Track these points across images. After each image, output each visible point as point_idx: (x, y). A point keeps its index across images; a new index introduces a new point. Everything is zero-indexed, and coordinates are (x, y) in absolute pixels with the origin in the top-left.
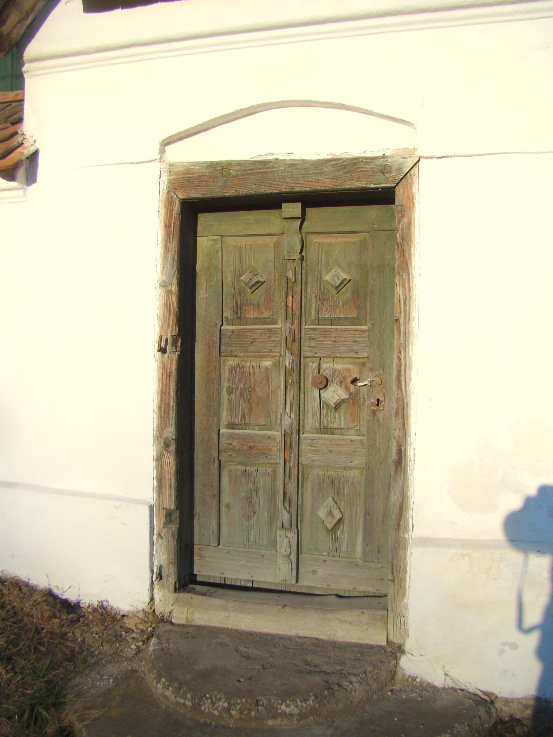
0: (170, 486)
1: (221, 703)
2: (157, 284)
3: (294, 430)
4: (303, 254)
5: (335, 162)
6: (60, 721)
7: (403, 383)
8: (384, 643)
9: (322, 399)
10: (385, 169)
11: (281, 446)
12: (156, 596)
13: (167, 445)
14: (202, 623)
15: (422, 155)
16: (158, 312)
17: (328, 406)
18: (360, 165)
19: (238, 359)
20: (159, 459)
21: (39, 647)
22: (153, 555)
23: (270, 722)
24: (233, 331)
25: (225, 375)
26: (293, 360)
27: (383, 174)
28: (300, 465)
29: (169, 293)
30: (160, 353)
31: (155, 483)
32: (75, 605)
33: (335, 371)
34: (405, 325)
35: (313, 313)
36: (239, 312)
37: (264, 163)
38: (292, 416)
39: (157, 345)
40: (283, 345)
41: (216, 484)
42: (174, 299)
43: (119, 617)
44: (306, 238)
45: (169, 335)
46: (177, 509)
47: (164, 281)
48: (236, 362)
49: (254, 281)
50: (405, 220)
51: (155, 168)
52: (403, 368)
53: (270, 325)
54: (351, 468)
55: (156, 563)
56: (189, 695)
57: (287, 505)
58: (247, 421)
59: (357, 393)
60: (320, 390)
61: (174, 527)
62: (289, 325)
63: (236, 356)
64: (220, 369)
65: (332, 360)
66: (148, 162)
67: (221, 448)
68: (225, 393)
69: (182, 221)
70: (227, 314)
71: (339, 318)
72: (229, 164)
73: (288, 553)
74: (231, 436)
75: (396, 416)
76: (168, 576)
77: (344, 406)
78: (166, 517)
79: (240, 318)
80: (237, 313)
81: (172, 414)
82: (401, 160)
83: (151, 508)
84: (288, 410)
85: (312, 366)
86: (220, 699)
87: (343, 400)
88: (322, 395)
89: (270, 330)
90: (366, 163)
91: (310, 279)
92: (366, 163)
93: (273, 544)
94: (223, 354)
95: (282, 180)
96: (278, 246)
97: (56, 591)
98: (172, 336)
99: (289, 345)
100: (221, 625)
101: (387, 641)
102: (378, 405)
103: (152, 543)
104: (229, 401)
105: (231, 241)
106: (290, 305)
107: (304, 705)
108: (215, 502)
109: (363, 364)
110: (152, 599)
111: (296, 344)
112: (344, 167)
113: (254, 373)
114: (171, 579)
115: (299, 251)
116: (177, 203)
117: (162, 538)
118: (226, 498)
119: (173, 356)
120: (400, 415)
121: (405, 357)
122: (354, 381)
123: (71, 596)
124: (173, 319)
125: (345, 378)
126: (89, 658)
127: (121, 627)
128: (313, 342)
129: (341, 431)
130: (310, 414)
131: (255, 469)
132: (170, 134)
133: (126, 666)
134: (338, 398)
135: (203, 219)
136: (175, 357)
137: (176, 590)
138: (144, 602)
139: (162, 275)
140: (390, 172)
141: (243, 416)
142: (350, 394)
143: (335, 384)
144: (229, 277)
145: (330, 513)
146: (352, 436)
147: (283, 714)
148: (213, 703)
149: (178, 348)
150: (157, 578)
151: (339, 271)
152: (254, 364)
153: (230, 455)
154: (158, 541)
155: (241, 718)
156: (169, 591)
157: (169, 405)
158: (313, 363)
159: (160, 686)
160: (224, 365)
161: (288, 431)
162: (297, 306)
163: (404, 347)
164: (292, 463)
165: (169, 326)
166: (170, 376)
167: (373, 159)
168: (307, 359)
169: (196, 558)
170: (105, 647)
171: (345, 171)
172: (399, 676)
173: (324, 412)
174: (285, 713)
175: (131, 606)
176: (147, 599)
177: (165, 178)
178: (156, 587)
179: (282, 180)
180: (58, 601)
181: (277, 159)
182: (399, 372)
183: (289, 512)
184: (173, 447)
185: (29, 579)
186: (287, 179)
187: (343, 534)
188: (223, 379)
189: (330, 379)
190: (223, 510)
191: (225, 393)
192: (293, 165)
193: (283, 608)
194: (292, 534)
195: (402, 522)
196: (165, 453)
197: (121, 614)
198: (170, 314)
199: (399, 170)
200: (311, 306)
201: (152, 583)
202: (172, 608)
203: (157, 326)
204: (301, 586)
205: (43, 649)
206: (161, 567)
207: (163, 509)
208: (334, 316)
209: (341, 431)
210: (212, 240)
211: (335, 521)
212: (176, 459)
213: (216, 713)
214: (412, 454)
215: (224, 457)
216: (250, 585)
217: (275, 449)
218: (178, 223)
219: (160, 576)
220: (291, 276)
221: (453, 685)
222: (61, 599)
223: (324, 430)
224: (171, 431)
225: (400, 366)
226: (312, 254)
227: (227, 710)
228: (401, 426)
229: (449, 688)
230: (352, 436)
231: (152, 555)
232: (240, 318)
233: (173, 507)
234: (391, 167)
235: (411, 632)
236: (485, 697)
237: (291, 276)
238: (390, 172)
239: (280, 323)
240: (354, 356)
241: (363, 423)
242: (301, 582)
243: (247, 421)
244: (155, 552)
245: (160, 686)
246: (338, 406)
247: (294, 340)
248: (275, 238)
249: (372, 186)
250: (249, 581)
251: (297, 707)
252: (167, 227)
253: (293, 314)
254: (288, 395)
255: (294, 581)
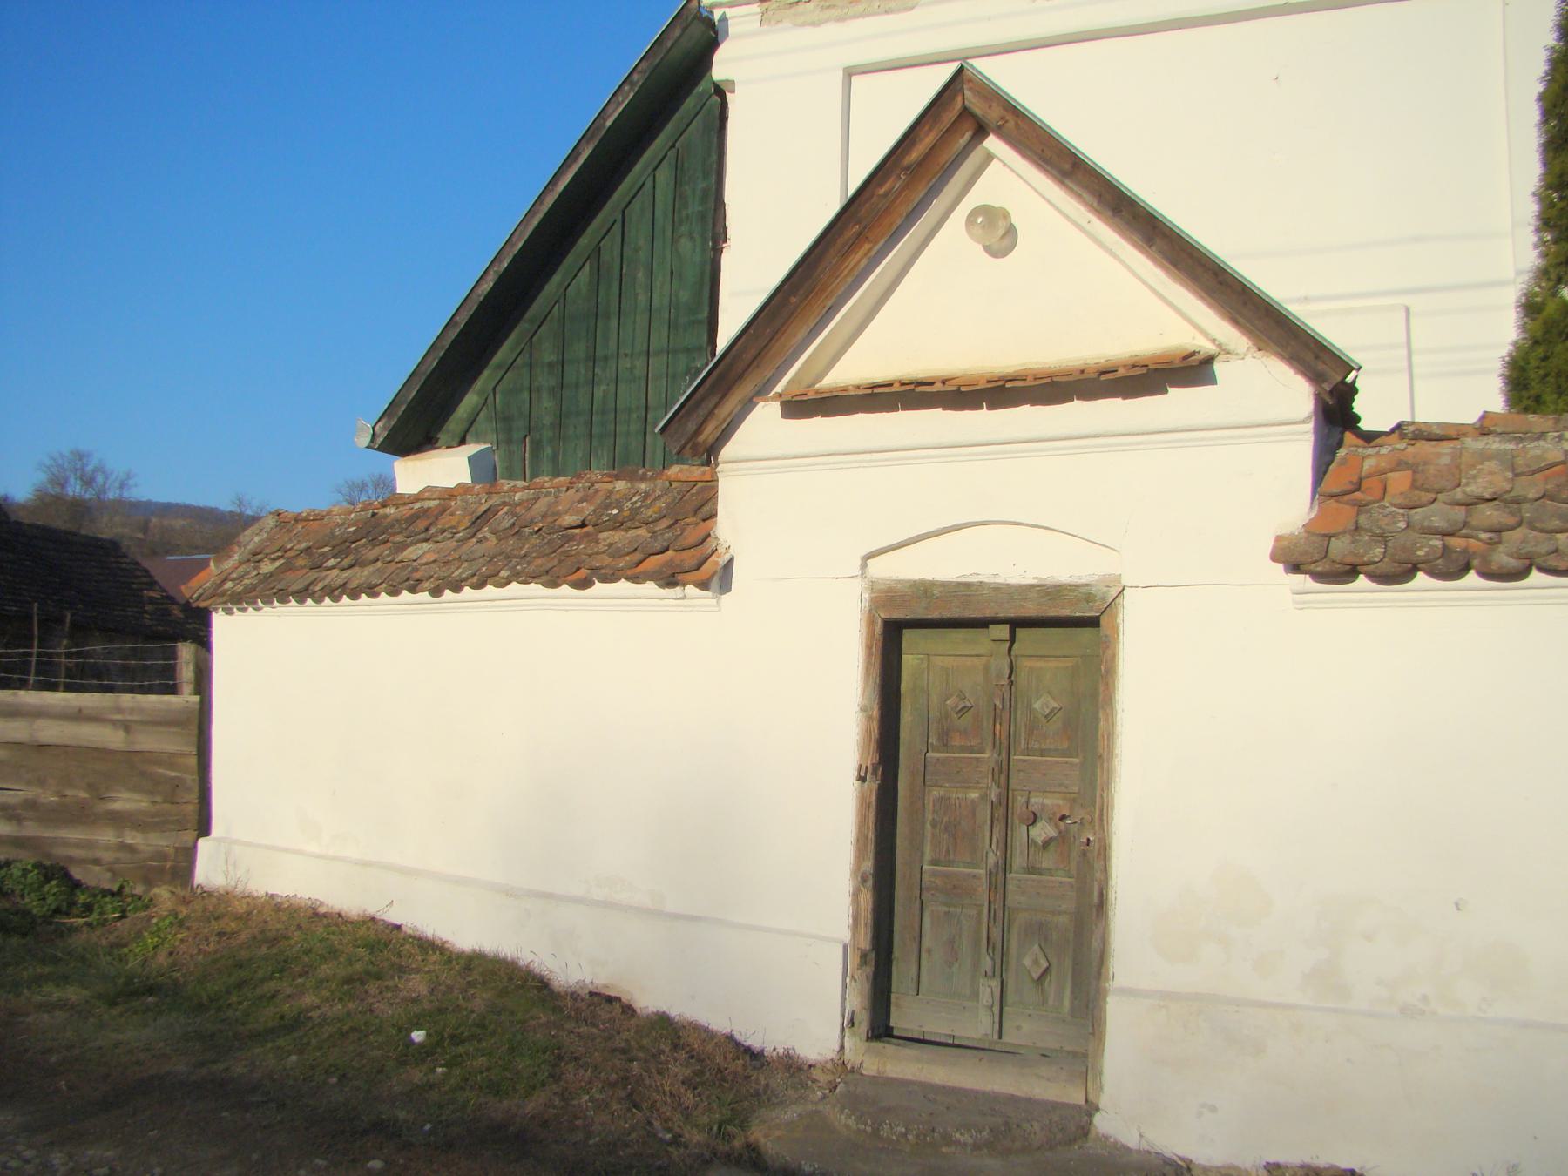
0: (866, 924)
1: (899, 1129)
2: (858, 709)
3: (1000, 869)
4: (1013, 679)
5: (1038, 588)
6: (746, 1138)
7: (1105, 823)
8: (1082, 1102)
9: (1030, 836)
10: (1089, 598)
11: (985, 886)
12: (846, 1045)
13: (864, 880)
14: (894, 1075)
15: (1126, 584)
16: (857, 737)
17: (1035, 844)
18: (1066, 592)
19: (943, 789)
20: (856, 895)
21: (722, 1083)
22: (845, 999)
23: (944, 1149)
24: (938, 759)
25: (929, 807)
26: (1000, 793)
27: (1088, 602)
28: (1006, 907)
29: (870, 718)
30: (859, 782)
31: (851, 921)
32: (758, 1053)
33: (1044, 806)
34: (1108, 762)
35: (1023, 742)
36: (945, 738)
37: (967, 585)
38: (998, 853)
39: (856, 774)
40: (990, 776)
41: (917, 929)
42: (875, 725)
43: (805, 1068)
44: (1016, 661)
45: (869, 762)
46: (873, 949)
47: (865, 706)
48: (942, 793)
49: (960, 707)
50: (1109, 652)
51: (856, 586)
52: (1105, 808)
53: (978, 753)
54: (1060, 913)
55: (848, 1007)
56: (869, 1122)
57: (991, 952)
58: (951, 857)
59: (1067, 831)
60: (1028, 826)
61: (870, 969)
62: (995, 755)
63: (941, 787)
64: (924, 800)
65: (1041, 794)
66: (849, 577)
67: (923, 886)
68: (928, 826)
69: (885, 639)
70: (933, 740)
71: (1049, 750)
72: (933, 583)
73: (990, 1003)
74: (934, 874)
75: (1097, 858)
76: (860, 1023)
77: (1052, 845)
78: (861, 957)
79: (945, 745)
80: (943, 740)
81: (871, 848)
82: (1105, 589)
83: (845, 948)
84: (994, 847)
85: (1021, 799)
86: (898, 1125)
87: (1051, 838)
88: (1030, 832)
89: (977, 759)
90: (1070, 591)
91: (1019, 706)
92: (1070, 591)
93: (975, 995)
94: (927, 783)
95: (986, 604)
96: (986, 669)
97: (738, 1037)
98: (873, 764)
99: (996, 777)
100: (914, 1079)
101: (1087, 1101)
102: (1088, 845)
103: (845, 986)
104: (933, 834)
105: (938, 661)
106: (998, 733)
107: (979, 1136)
108: (915, 946)
109: (1074, 800)
110: (842, 1047)
111: (1003, 777)
112: (1048, 594)
113: (960, 806)
114: (863, 1026)
115: (1007, 676)
116: (879, 628)
117: (855, 980)
118: (927, 942)
119: (873, 785)
120: (1102, 857)
121: (1108, 796)
122: (1063, 818)
123: (754, 1042)
124: (873, 746)
125: (1054, 814)
126: (773, 1098)
127: (808, 1077)
128: (1021, 773)
129: (1049, 872)
130: (1018, 852)
131: (959, 910)
132: (874, 549)
133: (810, 1107)
134: (1044, 835)
135: (909, 636)
136: (875, 786)
137: (868, 1039)
138: (833, 1050)
139: (863, 699)
140: (1095, 601)
141: (948, 851)
142: (1060, 832)
143: (1043, 821)
144: (935, 699)
145: (1036, 962)
146: (1061, 878)
147: (957, 1143)
148: (891, 1128)
149: (879, 777)
150: (848, 1024)
151: (1049, 698)
152: (960, 796)
153: (933, 894)
154: (850, 983)
155: (917, 1144)
156: (861, 1040)
157: (867, 838)
158: (1022, 796)
159: (843, 1117)
160: (929, 795)
161: (994, 871)
162: (1005, 735)
163: (1107, 784)
164: (998, 905)
165: (869, 754)
166: (869, 807)
167: (1077, 586)
168: (1016, 793)
169: (893, 1008)
170: (790, 1092)
171: (1049, 597)
172: (1092, 1135)
173: (1032, 850)
174: (959, 1142)
175: (819, 1054)
176: (837, 1048)
177: (866, 595)
178: (847, 1034)
179: (986, 604)
180: (742, 1049)
181: (981, 582)
182: (1102, 810)
183: (993, 959)
184: (870, 883)
185: (709, 1024)
186: (992, 604)
187: (1051, 984)
188: (927, 811)
189: (1038, 815)
190: (924, 955)
191: (928, 826)
192: (997, 589)
193: (980, 1060)
194: (995, 984)
195: (1103, 971)
196: (863, 889)
197: (808, 1063)
198: (870, 741)
199: (1103, 599)
200: (1020, 736)
201: (843, 1029)
202: (863, 1058)
203: (857, 753)
204: (1005, 1044)
205: (726, 1085)
206: (853, 1013)
207: (858, 949)
208: (1044, 747)
209: (1049, 872)
210: (918, 659)
211: (1041, 971)
212: (874, 895)
213: (894, 1138)
214: (1113, 898)
215: (926, 896)
216: (950, 1041)
217: (980, 889)
218: (880, 645)
219: (852, 1023)
220: (998, 703)
221: (1150, 1149)
222: (743, 1046)
223: (1031, 869)
224: (868, 865)
225: (1103, 805)
226: (1022, 678)
227: (905, 1135)
228: (1103, 868)
229: (1144, 1151)
230: (1061, 878)
231: (844, 999)
232: (945, 745)
233: (868, 947)
234: (1096, 596)
235: (1106, 1089)
236: (1179, 1162)
237: (998, 703)
238: (1095, 601)
239: (987, 751)
240: (1066, 790)
241: (1073, 865)
242: (1005, 1039)
243: (951, 857)
244: (847, 996)
245: (843, 1117)
246: (1046, 844)
247: (1001, 772)
248: (983, 660)
249: (1077, 614)
250: (949, 1036)
251: (971, 1137)
252: (869, 647)
253: (1000, 743)
254: (994, 830)
255: (996, 1036)
